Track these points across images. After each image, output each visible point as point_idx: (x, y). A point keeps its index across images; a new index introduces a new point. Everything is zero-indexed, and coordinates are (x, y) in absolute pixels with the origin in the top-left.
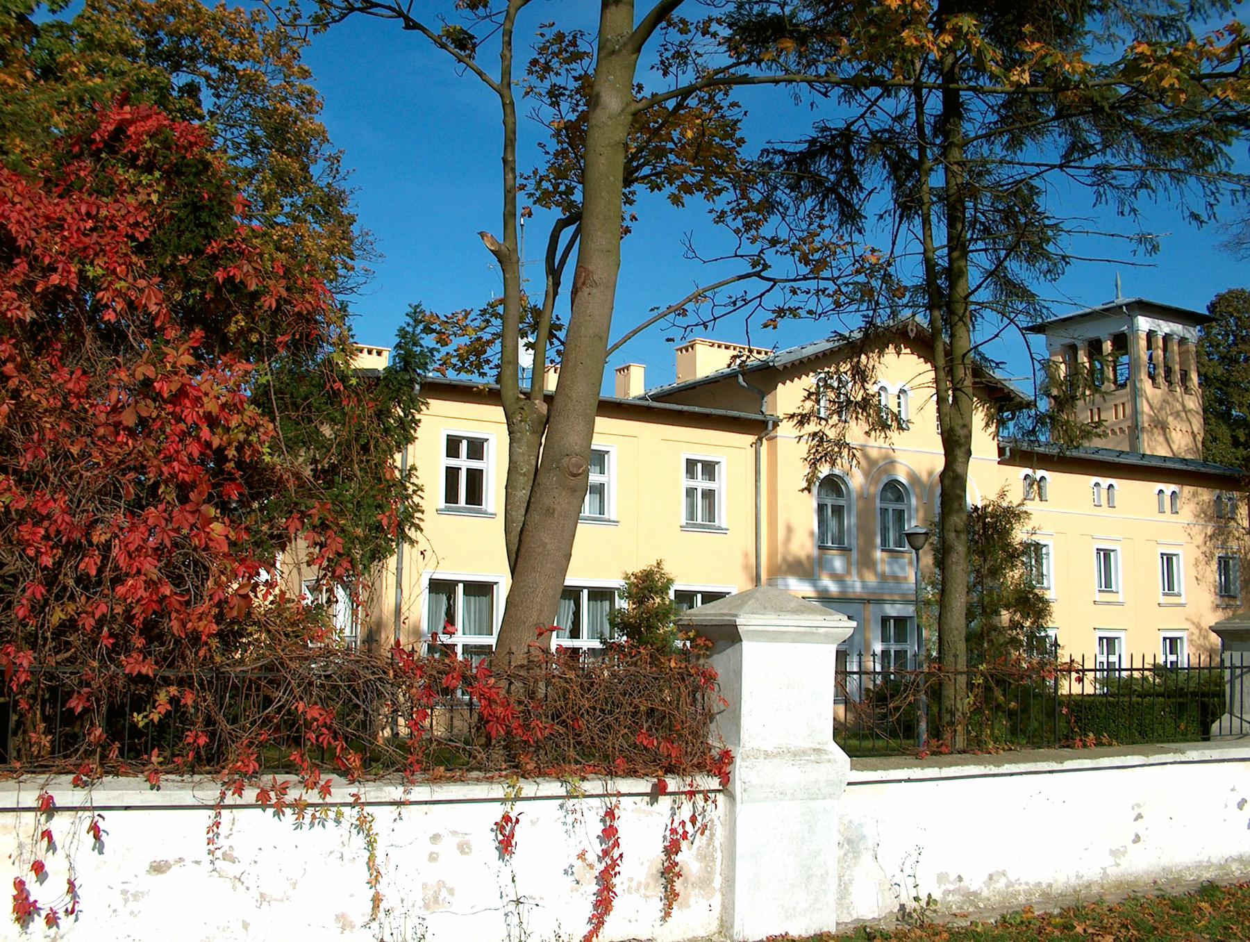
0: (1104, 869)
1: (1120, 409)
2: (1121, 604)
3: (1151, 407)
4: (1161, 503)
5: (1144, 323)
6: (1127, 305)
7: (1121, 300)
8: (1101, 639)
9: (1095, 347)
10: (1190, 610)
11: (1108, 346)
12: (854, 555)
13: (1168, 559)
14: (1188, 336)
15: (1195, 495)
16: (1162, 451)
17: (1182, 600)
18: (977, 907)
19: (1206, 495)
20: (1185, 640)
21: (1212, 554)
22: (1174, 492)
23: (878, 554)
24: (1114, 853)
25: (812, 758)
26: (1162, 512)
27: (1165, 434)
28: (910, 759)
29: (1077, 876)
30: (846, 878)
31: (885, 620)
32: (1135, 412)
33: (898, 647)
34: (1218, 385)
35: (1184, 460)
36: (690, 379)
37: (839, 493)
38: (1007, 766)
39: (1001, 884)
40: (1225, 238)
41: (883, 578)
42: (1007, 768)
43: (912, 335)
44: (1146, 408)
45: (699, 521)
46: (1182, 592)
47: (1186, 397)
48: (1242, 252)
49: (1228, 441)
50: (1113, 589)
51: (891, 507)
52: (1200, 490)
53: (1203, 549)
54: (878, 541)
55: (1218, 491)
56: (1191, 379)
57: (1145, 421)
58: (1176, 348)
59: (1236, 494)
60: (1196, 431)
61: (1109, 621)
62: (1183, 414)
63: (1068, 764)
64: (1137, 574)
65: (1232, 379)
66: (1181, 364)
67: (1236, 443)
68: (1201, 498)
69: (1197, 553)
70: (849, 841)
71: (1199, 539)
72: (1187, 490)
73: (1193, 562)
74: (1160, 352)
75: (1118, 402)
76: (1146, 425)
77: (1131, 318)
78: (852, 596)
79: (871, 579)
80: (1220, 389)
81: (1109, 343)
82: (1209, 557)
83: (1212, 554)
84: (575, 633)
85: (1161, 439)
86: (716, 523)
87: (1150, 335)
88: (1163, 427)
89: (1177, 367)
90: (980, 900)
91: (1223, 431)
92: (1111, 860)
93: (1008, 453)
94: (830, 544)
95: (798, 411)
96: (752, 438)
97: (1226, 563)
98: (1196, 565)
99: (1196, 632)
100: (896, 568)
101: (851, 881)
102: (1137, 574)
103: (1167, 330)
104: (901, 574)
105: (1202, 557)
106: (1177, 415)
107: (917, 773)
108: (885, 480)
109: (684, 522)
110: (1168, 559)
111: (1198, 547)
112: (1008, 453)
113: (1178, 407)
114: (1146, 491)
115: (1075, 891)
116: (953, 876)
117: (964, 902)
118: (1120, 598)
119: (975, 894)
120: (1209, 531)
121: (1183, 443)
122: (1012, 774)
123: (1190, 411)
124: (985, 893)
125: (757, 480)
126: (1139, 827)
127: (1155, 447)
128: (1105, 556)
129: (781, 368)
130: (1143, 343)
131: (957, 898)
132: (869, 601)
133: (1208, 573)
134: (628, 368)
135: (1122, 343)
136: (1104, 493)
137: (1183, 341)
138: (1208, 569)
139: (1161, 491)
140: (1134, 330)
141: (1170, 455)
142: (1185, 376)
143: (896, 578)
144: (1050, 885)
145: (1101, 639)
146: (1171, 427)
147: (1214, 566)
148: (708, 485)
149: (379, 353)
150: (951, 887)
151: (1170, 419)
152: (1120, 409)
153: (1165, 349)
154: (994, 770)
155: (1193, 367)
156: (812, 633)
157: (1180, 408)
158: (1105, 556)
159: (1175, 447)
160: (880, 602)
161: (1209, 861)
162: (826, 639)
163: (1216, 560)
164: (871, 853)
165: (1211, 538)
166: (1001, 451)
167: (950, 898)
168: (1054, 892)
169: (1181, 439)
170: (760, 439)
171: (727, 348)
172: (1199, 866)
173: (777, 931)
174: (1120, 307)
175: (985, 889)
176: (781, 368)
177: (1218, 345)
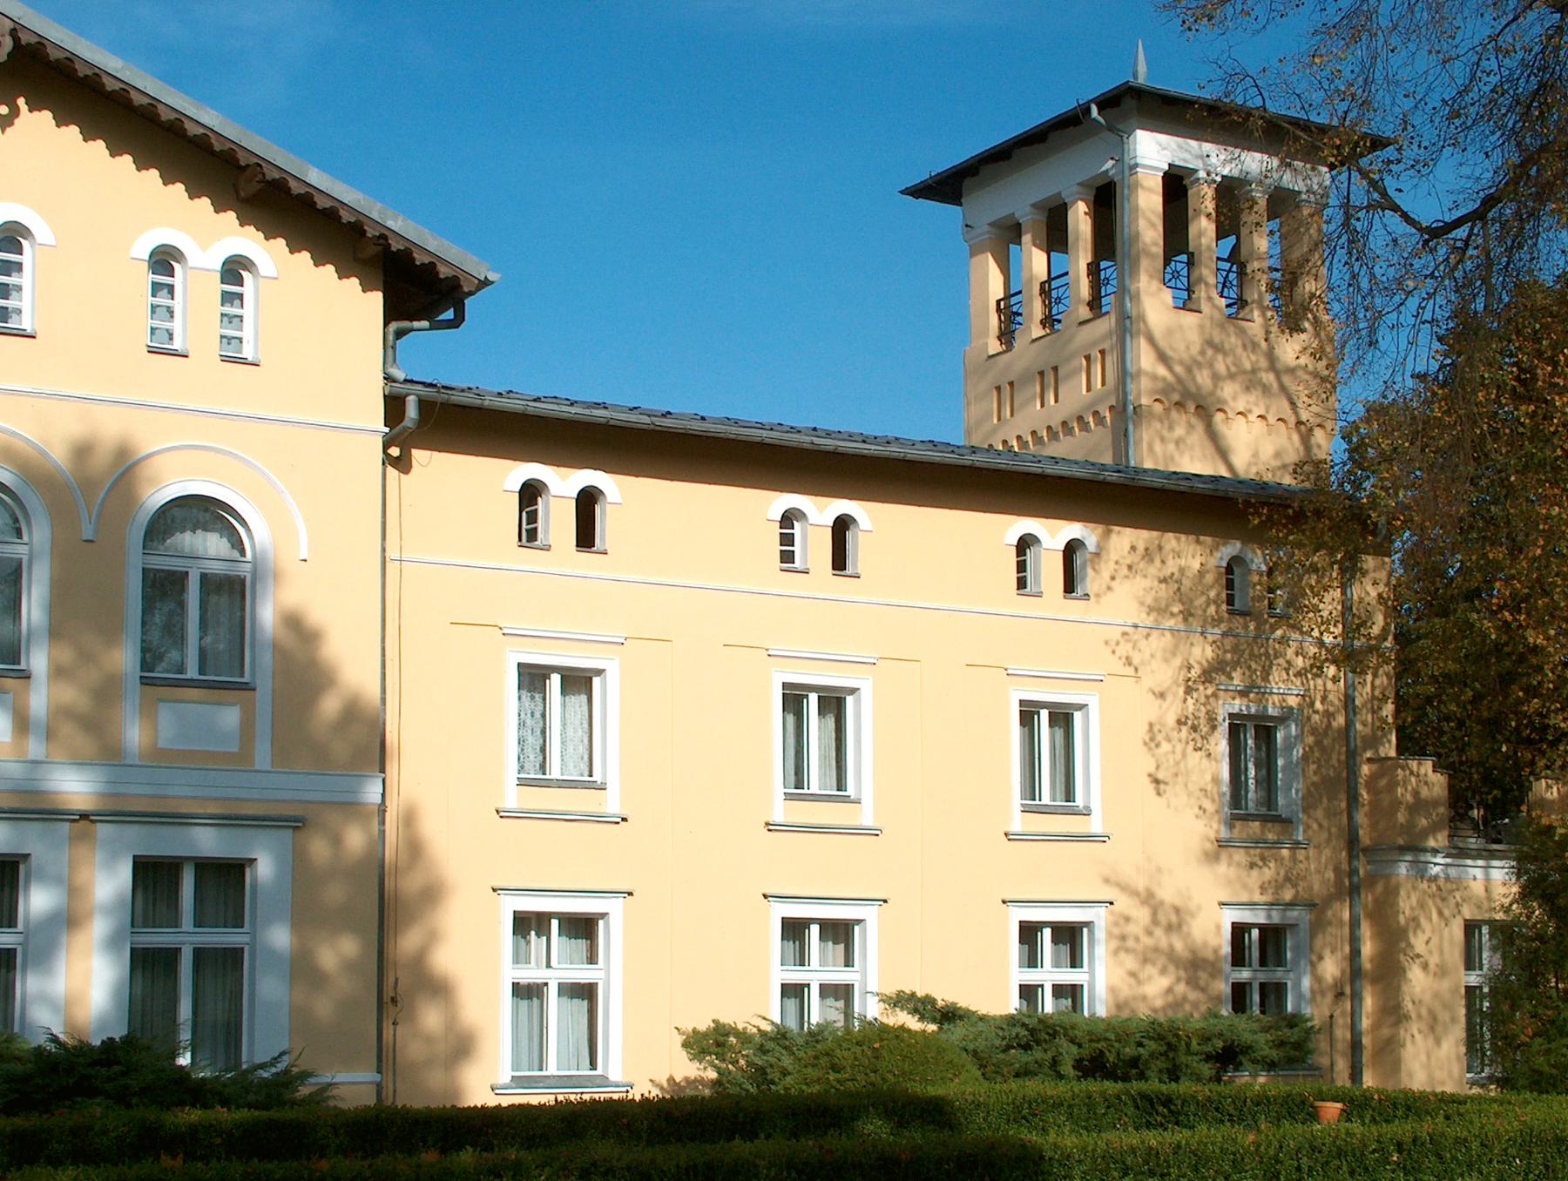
2: (1101, 839)
3: (1163, 358)
5: (1153, 151)
10: (1124, 857)
11: (1080, 219)
17: (1095, 825)
20: (1100, 934)
22: (1071, 550)
32: (1124, 375)
45: (1046, 800)
46: (1096, 806)
52: (1171, 540)
57: (1143, 394)
62: (1269, 378)
64: (932, 755)
71: (1164, 674)
72: (1125, 540)
73: (1142, 732)
77: (1119, 134)
85: (1198, 436)
88: (1205, 410)
93: (412, 411)
99: (1142, 915)
102: (932, 755)
106: (1251, 382)
112: (412, 411)
120: (1202, 652)
121: (1267, 450)
123: (1291, 371)
166: (393, 406)
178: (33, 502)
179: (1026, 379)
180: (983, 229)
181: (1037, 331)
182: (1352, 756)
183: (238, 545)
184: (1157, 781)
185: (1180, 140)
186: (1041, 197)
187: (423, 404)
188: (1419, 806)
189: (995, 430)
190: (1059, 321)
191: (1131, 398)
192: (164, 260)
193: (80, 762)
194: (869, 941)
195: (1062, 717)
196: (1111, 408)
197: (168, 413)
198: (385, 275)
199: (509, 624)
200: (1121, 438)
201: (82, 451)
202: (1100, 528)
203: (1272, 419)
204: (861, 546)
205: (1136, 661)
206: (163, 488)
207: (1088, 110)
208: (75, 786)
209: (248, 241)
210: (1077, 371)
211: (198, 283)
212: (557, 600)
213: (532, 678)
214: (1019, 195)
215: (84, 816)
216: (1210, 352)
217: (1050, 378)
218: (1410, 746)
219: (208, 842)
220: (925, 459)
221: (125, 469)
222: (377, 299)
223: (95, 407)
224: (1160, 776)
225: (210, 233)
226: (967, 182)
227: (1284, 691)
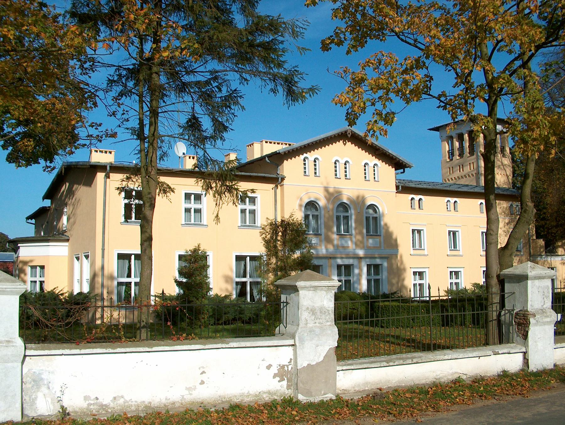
0: (183, 396)
2: (462, 256)
8: (451, 272)
9: (460, 138)
11: (466, 137)
12: (323, 236)
18: (107, 411)
23: (335, 237)
24: (188, 389)
25: (4, 345)
28: (74, 345)
29: (166, 399)
30: (33, 397)
31: (339, 267)
33: (346, 278)
36: (249, 159)
37: (316, 209)
38: (118, 349)
39: (121, 401)
41: (337, 247)
42: (118, 350)
43: (349, 136)
46: (461, 250)
47: (503, 159)
50: (458, 249)
51: (342, 215)
52: (502, 202)
54: (335, 229)
56: (506, 150)
60: (508, 174)
61: (455, 264)
62: (502, 167)
63: (155, 349)
68: (502, 206)
70: (34, 381)
75: (471, 162)
78: (321, 256)
79: (331, 248)
81: (467, 135)
84: (129, 276)
86: (256, 225)
90: (109, 408)
92: (187, 392)
93: (400, 188)
94: (311, 232)
95: (120, 186)
96: (273, 186)
100: (343, 242)
101: (36, 398)
104: (346, 245)
107: (67, 351)
109: (240, 225)
112: (400, 188)
115: (165, 405)
116: (93, 397)
117: (100, 409)
118: (461, 253)
119: (106, 405)
120: (507, 221)
121: (502, 180)
122: (126, 353)
123: (505, 165)
124: (112, 405)
125: (276, 204)
126: (204, 377)
128: (453, 234)
129: (283, 154)
131: (96, 407)
132: (330, 258)
134: (229, 154)
143: (343, 247)
144: (150, 403)
145: (451, 272)
148: (252, 207)
149: (110, 153)
150: (92, 402)
154: (111, 351)
156: (4, 291)
157: (501, 164)
158: (453, 234)
160: (335, 258)
161: (248, 392)
162: (12, 293)
164: (46, 386)
165: (507, 224)
166: (397, 187)
167: (92, 407)
168: (152, 406)
170: (277, 186)
171: (278, 144)
172: (242, 395)
173: (9, 419)
175: (112, 404)
176: (283, 154)
178: (352, 206)
179: (456, 166)
180: (444, 137)
182: (529, 239)
183: (376, 212)
188: (541, 247)
189: (449, 176)
192: (366, 164)
193: (361, 249)
194: (462, 276)
195: (454, 233)
201: (358, 197)
206: (369, 203)
208: (361, 253)
209: (376, 161)
210: (467, 165)
211: (370, 170)
212: (417, 219)
215: (361, 258)
217: (461, 166)
218: (538, 236)
219: (378, 261)
221: (363, 200)
222: (394, 169)
225: (372, 160)
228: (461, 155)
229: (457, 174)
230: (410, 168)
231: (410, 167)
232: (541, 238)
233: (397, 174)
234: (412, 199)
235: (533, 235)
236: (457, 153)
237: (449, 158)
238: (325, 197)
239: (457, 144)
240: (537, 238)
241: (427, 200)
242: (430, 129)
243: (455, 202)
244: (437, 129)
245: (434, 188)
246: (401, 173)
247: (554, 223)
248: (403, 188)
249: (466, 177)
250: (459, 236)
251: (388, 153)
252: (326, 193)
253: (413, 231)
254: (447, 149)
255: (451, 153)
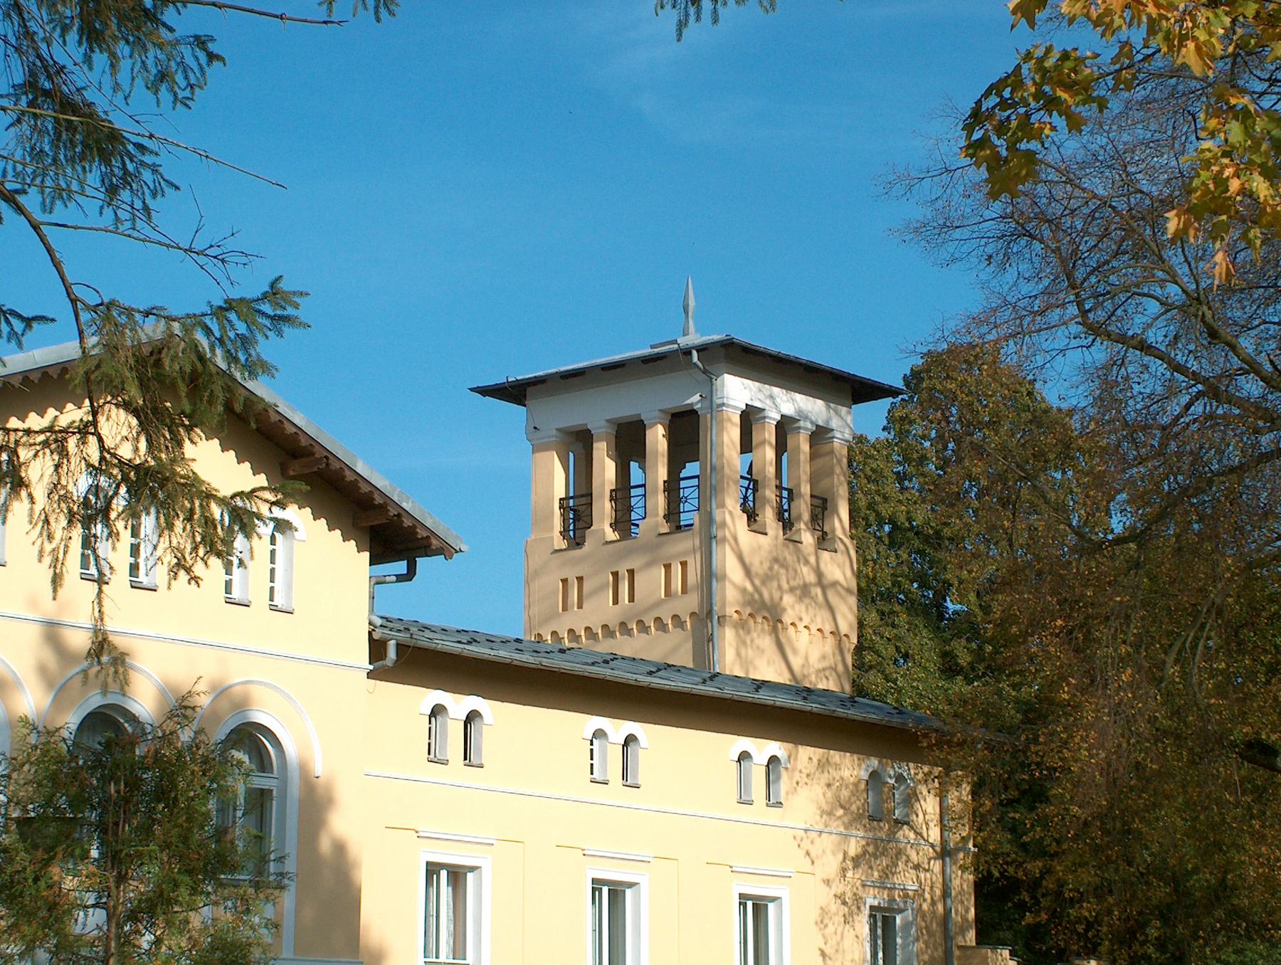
1: (677, 570)
4: (743, 783)
5: (737, 391)
6: (702, 349)
7: (693, 338)
9: (629, 442)
11: (657, 438)
13: (757, 909)
14: (835, 423)
15: (823, 765)
16: (769, 670)
19: (850, 768)
21: (858, 900)
22: (773, 760)
26: (745, 801)
27: (774, 631)
32: (710, 575)
34: (917, 543)
35: (807, 693)
40: (917, 212)
44: (734, 571)
47: (825, 555)
48: (951, 247)
49: (931, 659)
52: (835, 756)
53: (838, 888)
55: (874, 762)
58: (805, 447)
59: (912, 770)
65: (947, 532)
66: (813, 481)
67: (950, 669)
68: (837, 775)
69: (825, 896)
71: (831, 864)
72: (807, 755)
73: (815, 915)
74: (770, 454)
76: (730, 611)
77: (709, 377)
80: (921, 552)
81: (660, 430)
82: (851, 904)
83: (858, 900)
85: (767, 642)
87: (750, 417)
88: (772, 616)
89: (806, 489)
91: (923, 642)
93: (392, 653)
97: (888, 923)
98: (822, 923)
103: (788, 409)
105: (835, 906)
106: (803, 592)
108: (95, 700)
110: (757, 909)
111: (827, 882)
112: (392, 653)
113: (808, 575)
114: (708, 753)
120: (854, 848)
123: (835, 584)
127: (747, 659)
128: (612, 896)
130: (732, 434)
133: (849, 940)
135: (687, 432)
136: (615, 754)
137: (820, 435)
138: (849, 934)
139: (744, 756)
140: (716, 408)
141: (782, 677)
142: (821, 507)
146: (787, 619)
147: (863, 926)
151: (788, 600)
152: (677, 570)
153: (781, 448)
155: (843, 491)
157: (811, 578)
158: (612, 896)
159: (796, 663)
163: (866, 912)
165: (856, 861)
166: (377, 648)
169: (810, 646)
174: (687, 352)
177: (923, 459)
181: (611, 535)
184: (823, 954)
185: (757, 384)
186: (615, 416)
187: (399, 646)
190: (637, 525)
191: (715, 608)
196: (693, 614)
197: (245, 655)
198: (371, 540)
199: (426, 827)
200: (704, 643)
202: (790, 746)
203: (814, 629)
204: (644, 757)
205: (813, 854)
207: (690, 353)
213: (432, 870)
214: (598, 411)
216: (776, 567)
220: (702, 693)
222: (366, 556)
223: (229, 654)
224: (827, 951)
226: (529, 390)
227: (907, 879)
228: (623, 523)
229: (601, 610)
230: (448, 556)
231: (446, 550)
232: (1004, 944)
233: (378, 582)
234: (437, 711)
235: (963, 931)
236: (604, 510)
237: (564, 533)
238: (43, 670)
239: (606, 470)
240: (982, 939)
241: (504, 719)
242: (485, 391)
243: (630, 740)
244: (514, 392)
245: (545, 662)
246: (400, 578)
247: (1088, 877)
248: (405, 657)
249: (643, 628)
250: (637, 907)
251: (350, 477)
252: (49, 657)
253: (432, 870)
254: (559, 491)
255: (577, 515)
